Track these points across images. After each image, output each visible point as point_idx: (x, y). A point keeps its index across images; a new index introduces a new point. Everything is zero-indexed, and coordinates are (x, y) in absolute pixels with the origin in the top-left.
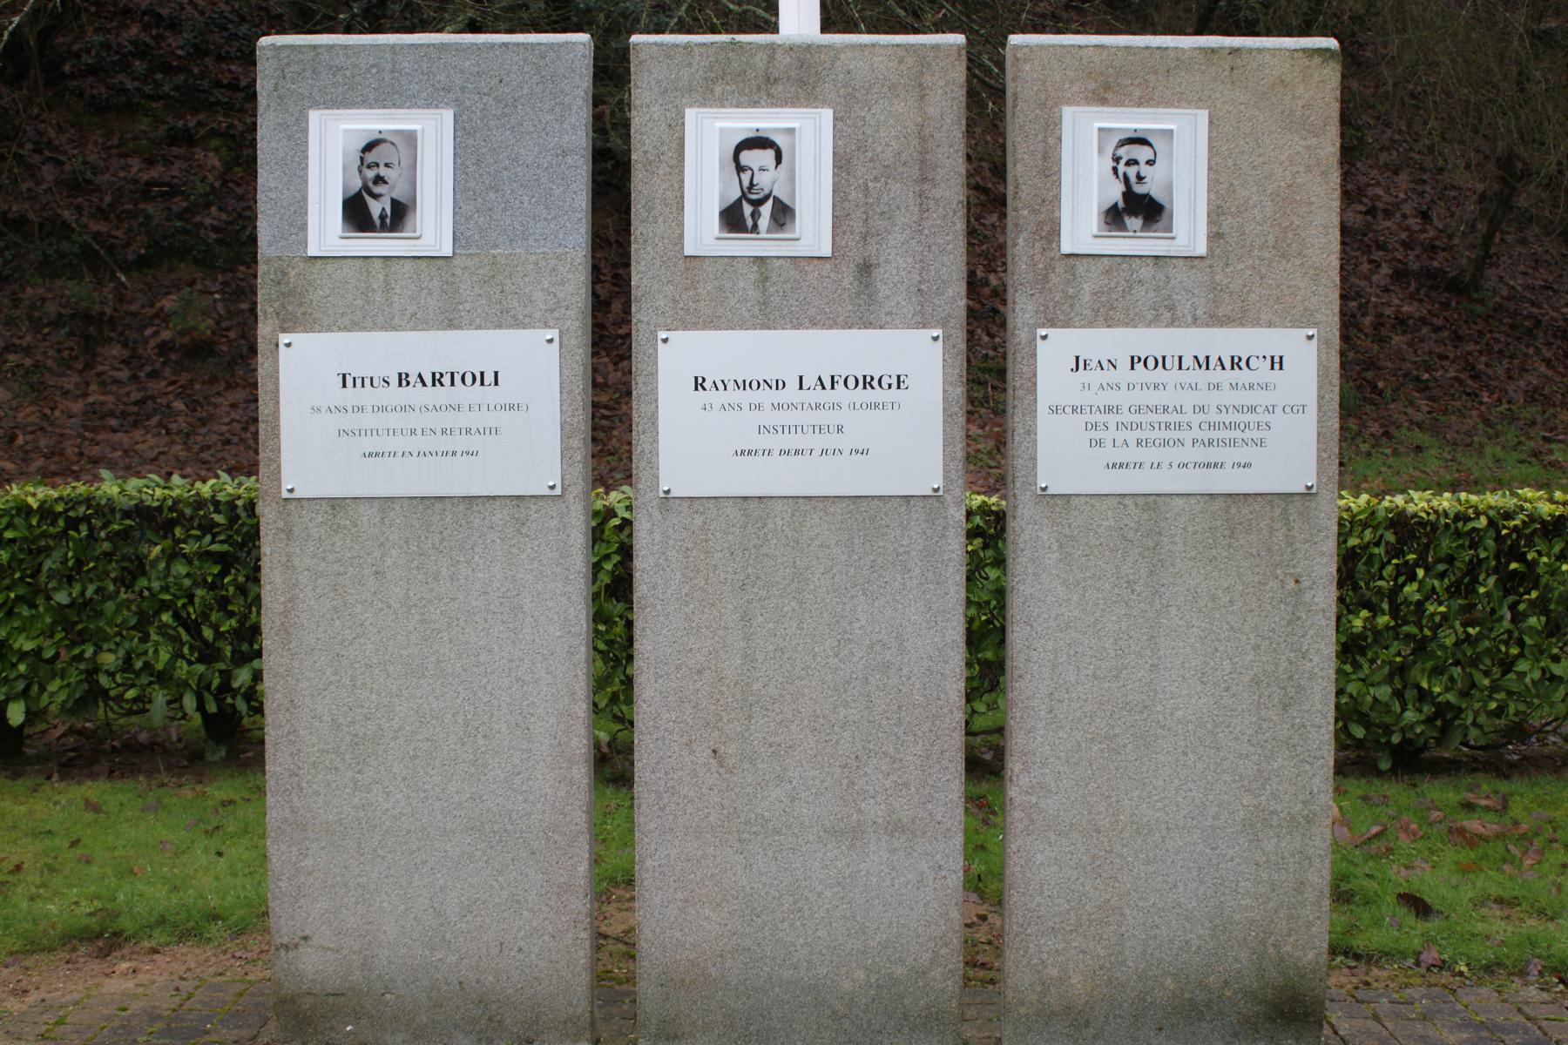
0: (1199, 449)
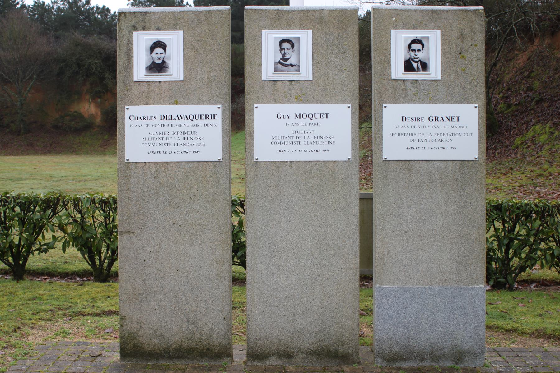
0: (421, 143)
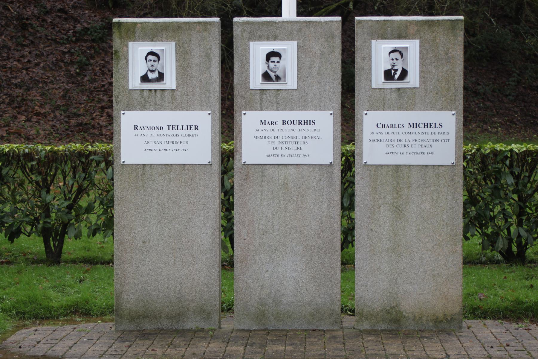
0: (440, 135)
